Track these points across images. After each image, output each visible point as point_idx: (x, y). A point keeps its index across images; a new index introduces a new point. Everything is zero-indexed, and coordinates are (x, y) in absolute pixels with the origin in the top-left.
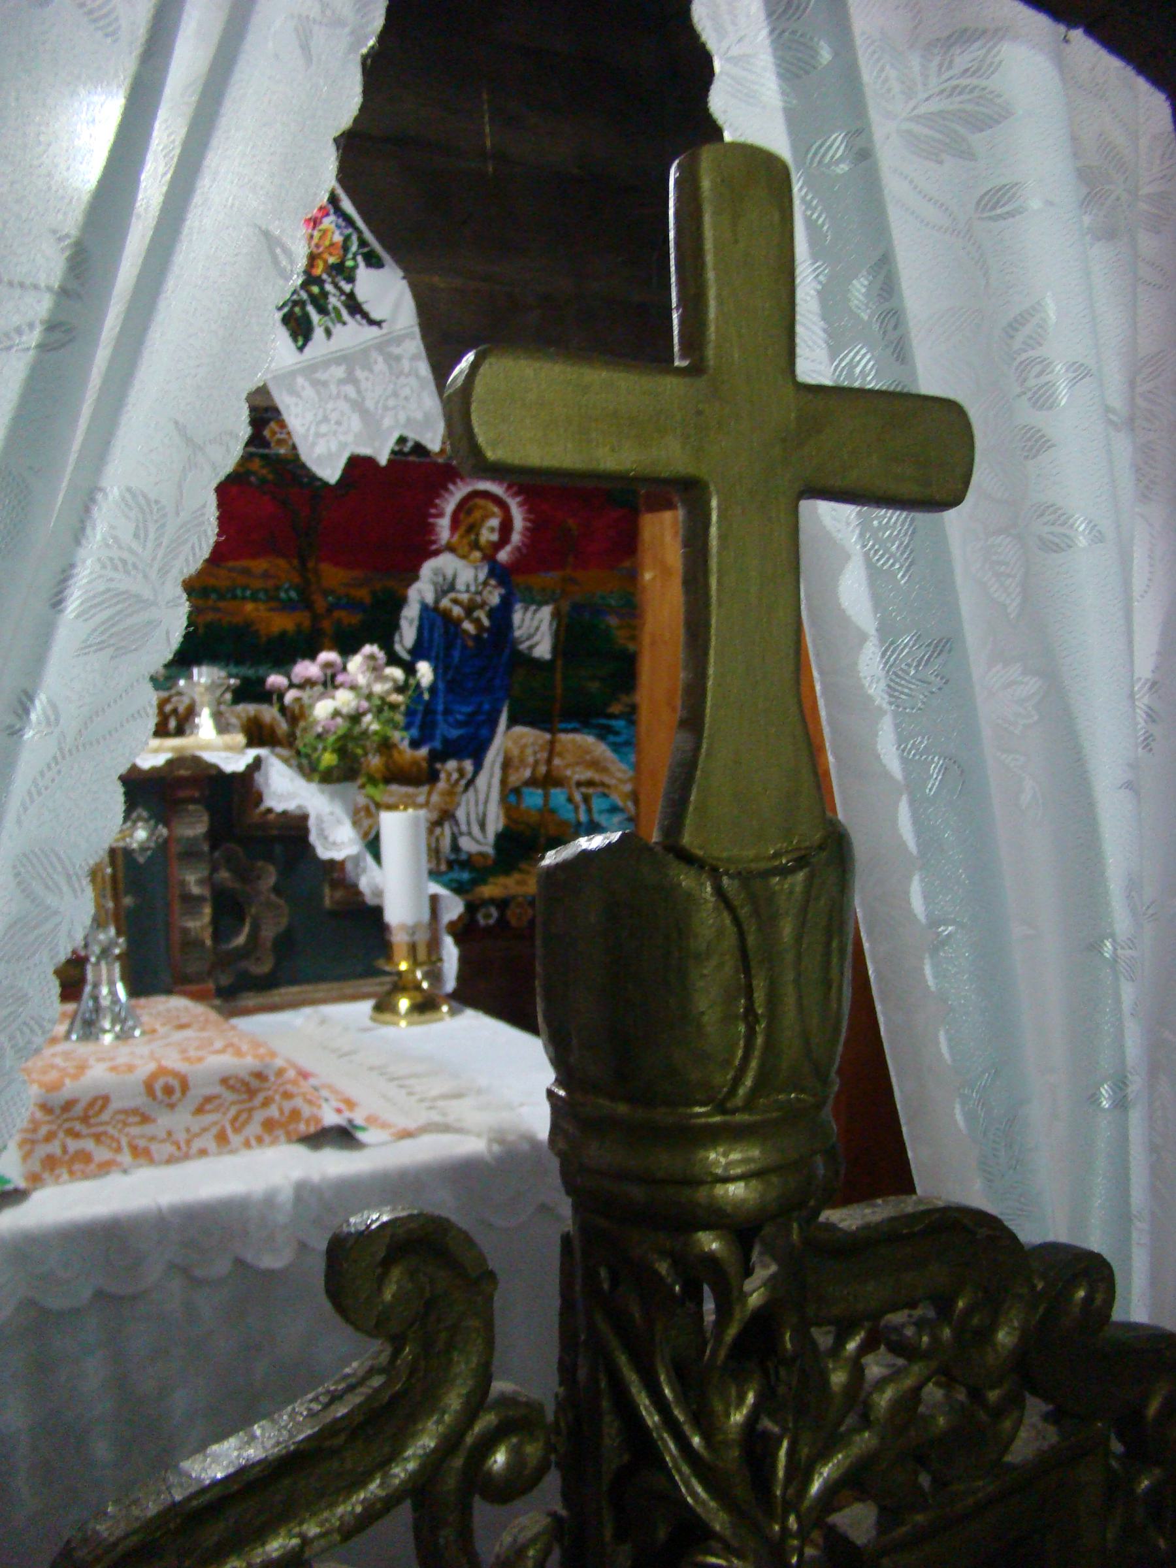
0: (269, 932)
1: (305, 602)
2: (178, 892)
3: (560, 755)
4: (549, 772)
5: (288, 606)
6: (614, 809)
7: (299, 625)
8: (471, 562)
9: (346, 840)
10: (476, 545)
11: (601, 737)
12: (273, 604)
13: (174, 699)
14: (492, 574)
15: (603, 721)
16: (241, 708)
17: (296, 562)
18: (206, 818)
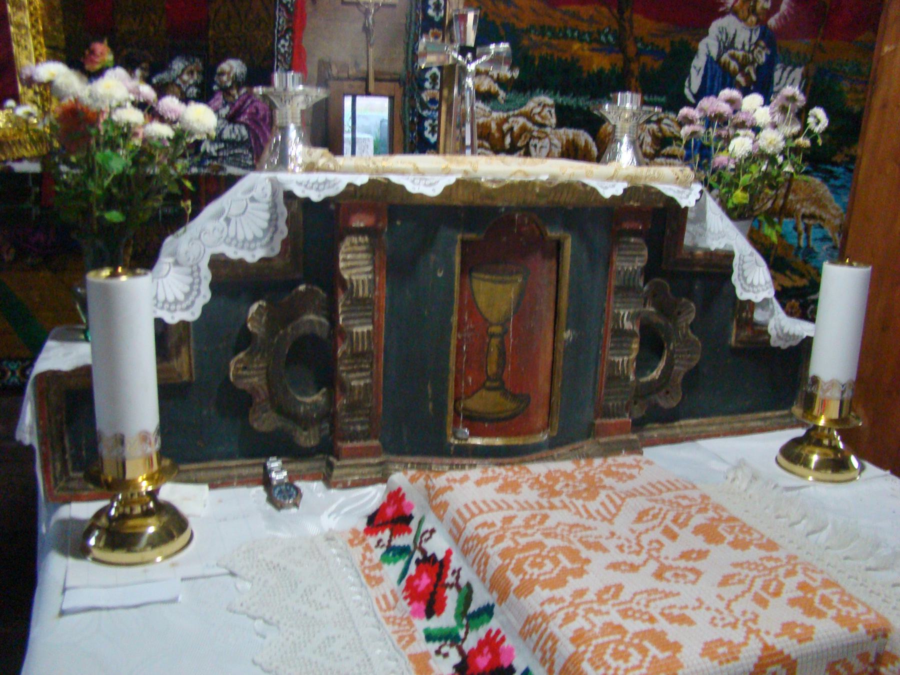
0: (680, 370)
1: (620, 46)
2: (610, 326)
3: (794, 191)
4: (784, 206)
5: (606, 49)
6: (825, 239)
7: (614, 66)
8: (748, 25)
9: (763, 282)
10: (753, 11)
11: (825, 180)
12: (595, 45)
13: (511, 120)
14: (762, 37)
15: (829, 167)
16: (562, 131)
17: (615, 11)
18: (645, 252)
